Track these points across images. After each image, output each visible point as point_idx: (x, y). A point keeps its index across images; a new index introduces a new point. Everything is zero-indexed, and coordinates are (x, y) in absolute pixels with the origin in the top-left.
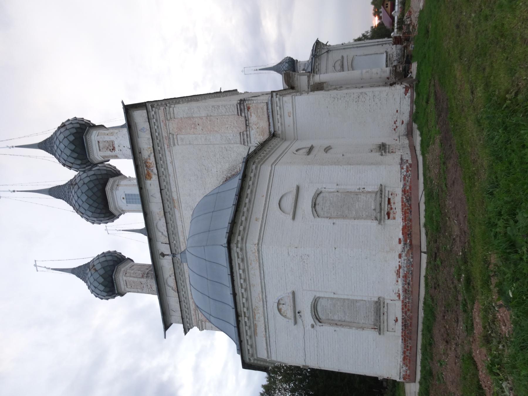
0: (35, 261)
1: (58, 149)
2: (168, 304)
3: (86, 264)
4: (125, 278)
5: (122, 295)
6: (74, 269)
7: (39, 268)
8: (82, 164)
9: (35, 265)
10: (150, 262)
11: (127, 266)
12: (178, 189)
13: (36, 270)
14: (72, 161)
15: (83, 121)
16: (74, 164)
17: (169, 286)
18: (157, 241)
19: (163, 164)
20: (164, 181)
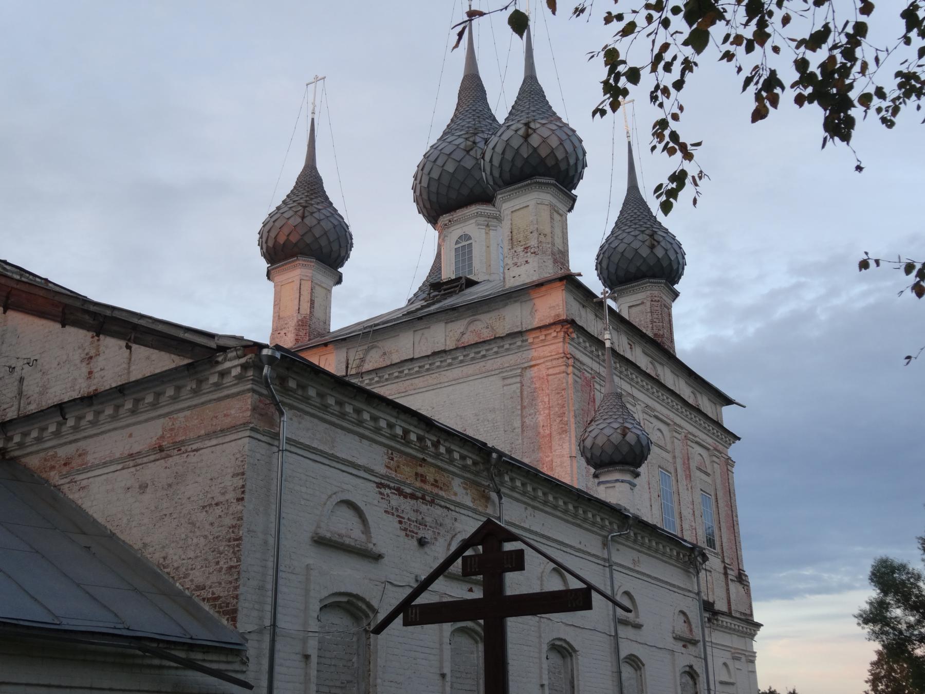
0: (324, 78)
1: (447, 144)
2: (398, 335)
3: (544, 97)
4: (532, 204)
5: (269, 276)
6: (315, 168)
7: (312, 87)
8: (429, 193)
9: (317, 79)
10: (336, 325)
11: (562, 207)
12: (424, 390)
13: (308, 82)
14: (497, 149)
15: (583, 168)
16: (492, 151)
17: (367, 351)
18: (415, 331)
19: (480, 355)
20: (453, 359)
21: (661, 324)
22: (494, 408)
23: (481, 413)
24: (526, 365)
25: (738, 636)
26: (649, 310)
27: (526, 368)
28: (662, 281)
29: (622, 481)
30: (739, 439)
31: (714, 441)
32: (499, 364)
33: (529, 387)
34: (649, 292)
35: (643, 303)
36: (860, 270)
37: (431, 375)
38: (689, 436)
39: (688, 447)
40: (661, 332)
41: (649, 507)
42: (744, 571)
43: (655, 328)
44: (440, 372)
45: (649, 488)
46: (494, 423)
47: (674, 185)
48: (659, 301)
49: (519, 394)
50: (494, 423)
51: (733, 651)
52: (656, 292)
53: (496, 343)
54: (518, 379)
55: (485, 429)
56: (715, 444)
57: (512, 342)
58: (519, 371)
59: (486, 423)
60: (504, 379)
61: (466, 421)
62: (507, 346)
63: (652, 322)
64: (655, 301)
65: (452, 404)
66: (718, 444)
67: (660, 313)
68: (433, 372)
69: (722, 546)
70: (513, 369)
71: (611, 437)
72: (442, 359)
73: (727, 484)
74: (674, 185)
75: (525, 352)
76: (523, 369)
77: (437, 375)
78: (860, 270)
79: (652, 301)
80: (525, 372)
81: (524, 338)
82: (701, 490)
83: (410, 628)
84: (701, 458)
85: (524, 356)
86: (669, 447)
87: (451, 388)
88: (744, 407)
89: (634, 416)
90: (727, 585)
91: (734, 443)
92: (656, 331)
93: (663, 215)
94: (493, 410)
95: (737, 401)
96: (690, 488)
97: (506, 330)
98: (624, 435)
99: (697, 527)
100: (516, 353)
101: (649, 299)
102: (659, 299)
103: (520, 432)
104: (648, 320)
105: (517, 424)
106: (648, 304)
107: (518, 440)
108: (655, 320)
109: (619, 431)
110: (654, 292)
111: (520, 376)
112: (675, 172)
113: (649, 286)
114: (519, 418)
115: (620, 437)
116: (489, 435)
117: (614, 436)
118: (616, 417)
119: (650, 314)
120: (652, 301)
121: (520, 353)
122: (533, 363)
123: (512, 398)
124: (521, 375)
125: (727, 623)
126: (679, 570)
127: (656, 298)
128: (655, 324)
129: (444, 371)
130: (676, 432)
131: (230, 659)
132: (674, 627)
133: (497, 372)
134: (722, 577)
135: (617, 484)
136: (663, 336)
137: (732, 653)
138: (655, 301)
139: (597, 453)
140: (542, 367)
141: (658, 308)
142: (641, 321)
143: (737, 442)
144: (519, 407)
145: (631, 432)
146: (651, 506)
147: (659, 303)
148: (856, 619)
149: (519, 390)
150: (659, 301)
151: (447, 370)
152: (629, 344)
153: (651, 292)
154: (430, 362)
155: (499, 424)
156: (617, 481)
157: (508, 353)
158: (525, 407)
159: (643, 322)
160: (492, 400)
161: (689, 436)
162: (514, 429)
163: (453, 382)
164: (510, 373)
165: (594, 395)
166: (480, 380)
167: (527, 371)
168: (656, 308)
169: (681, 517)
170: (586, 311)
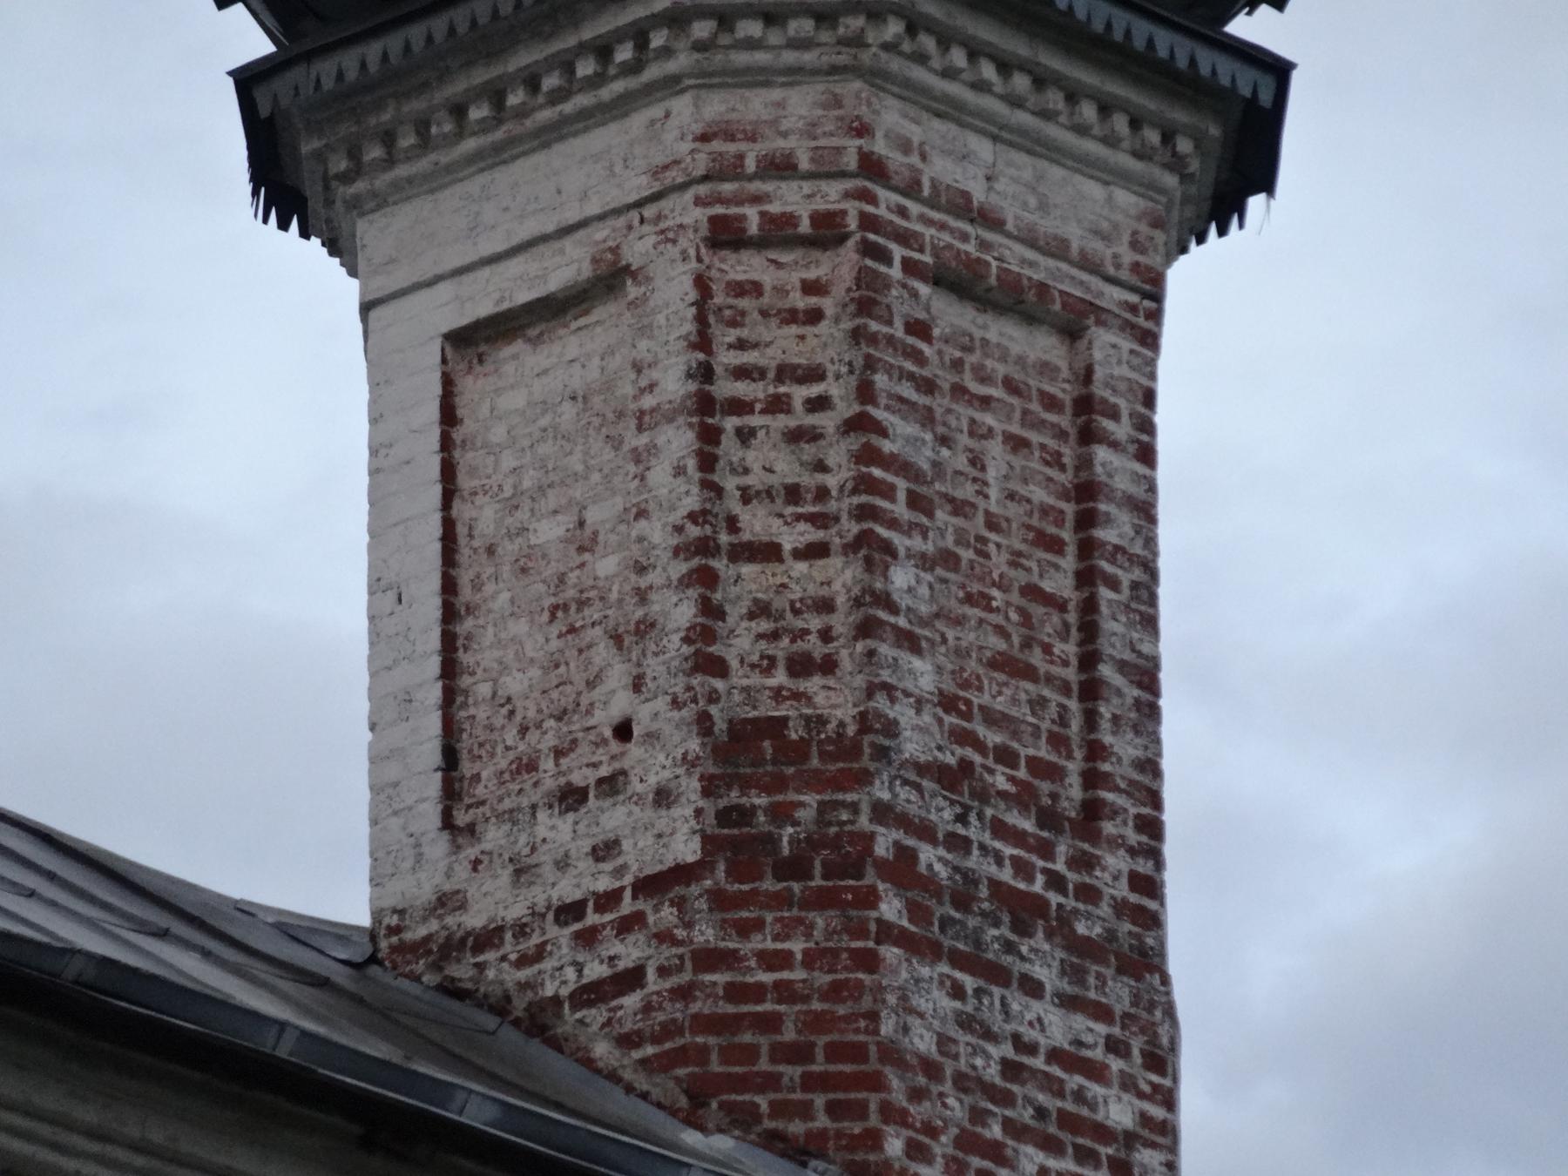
26: (673, 384)
36: (230, 73)
47: (918, 1125)
48: (828, 230)
52: (801, 103)
64: (779, 232)
67: (845, 408)
74: (918, 1125)
78: (230, 73)
83: (229, 86)
89: (474, 920)
101: (687, 212)
102: (832, 194)
104: (657, 532)
108: (757, 523)
110: (755, 104)
112: (1249, 13)
119: (678, 441)
128: (751, 579)
138: (779, 232)
147: (840, 266)
148: (505, 1024)
150: (828, 230)
153: (716, 106)
159: (606, 565)
168: (783, 344)
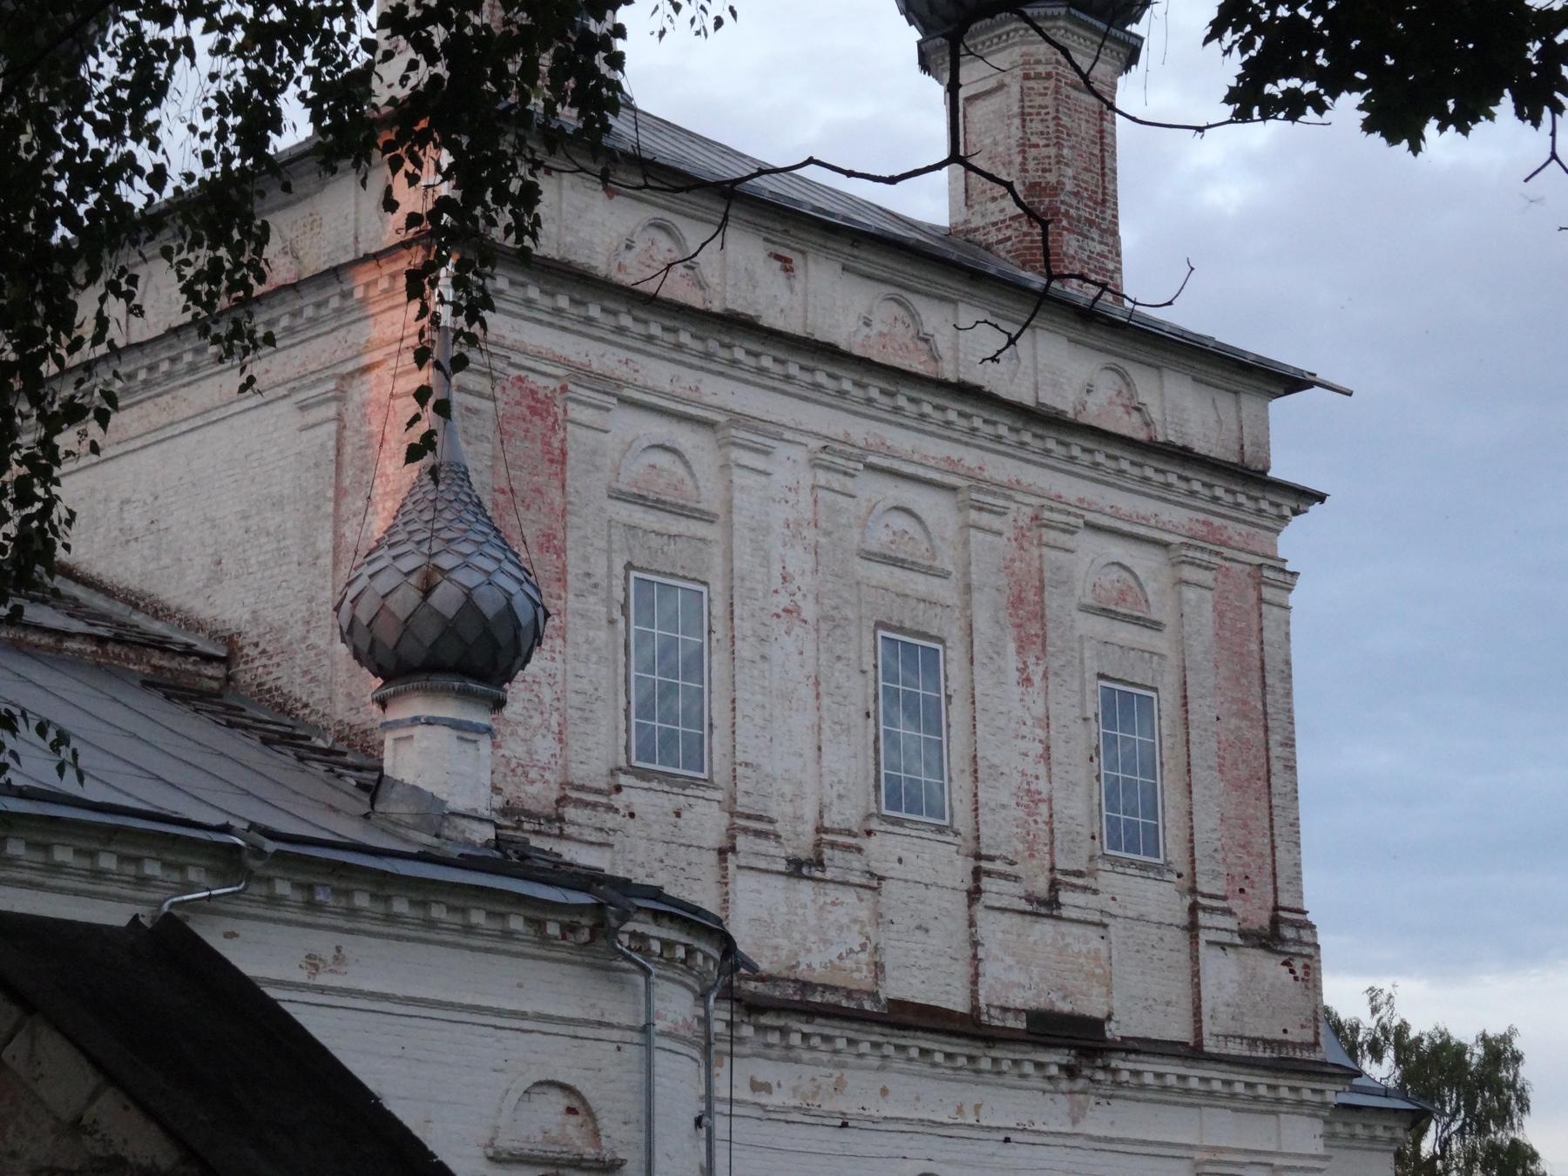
21: (1052, 151)
22: (282, 496)
23: (254, 511)
24: (350, 366)
25: (1236, 1110)
26: (1016, 109)
27: (351, 375)
28: (1056, 11)
29: (430, 722)
30: (1321, 498)
31: (1202, 516)
32: (297, 363)
33: (357, 431)
34: (1017, 50)
35: (1001, 87)
37: (158, 400)
38: (1047, 514)
39: (1045, 550)
40: (1052, 178)
41: (810, 753)
42: (1305, 913)
43: (1031, 165)
44: (173, 389)
45: (818, 696)
46: (279, 541)
48: (1049, 76)
49: (332, 454)
50: (279, 541)
51: (1198, 1156)
53: (283, 302)
54: (331, 410)
55: (261, 558)
56: (1205, 523)
57: (320, 298)
58: (331, 385)
59: (263, 540)
60: (303, 407)
61: (224, 533)
62: (309, 312)
63: (1025, 146)
64: (1038, 76)
65: (194, 485)
66: (1217, 521)
67: (1053, 114)
68: (159, 390)
69: (1191, 841)
70: (319, 380)
71: (390, 598)
72: (173, 353)
73: (1254, 647)
75: (353, 327)
76: (343, 377)
77: (167, 398)
79: (1027, 77)
80: (350, 386)
81: (346, 287)
82: (1101, 676)
84: (1125, 575)
85: (350, 339)
86: (945, 561)
87: (194, 437)
88: (1350, 394)
90: (1195, 959)
91: (1296, 512)
92: (1033, 176)
93: (201, 29)
94: (278, 504)
95: (1321, 376)
96: (1037, 679)
97: (323, 259)
98: (427, 590)
99: (1057, 795)
100: (333, 330)
101: (1019, 72)
102: (1049, 68)
103: (330, 567)
105: (325, 542)
106: (1015, 89)
107: (323, 588)
108: (1034, 139)
109: (414, 580)
110: (1032, 49)
111: (335, 399)
113: (1016, 30)
114: (329, 524)
115: (414, 597)
116: (268, 573)
117: (398, 595)
118: (463, 526)
119: (1017, 122)
120: (1027, 77)
121: (342, 333)
122: (365, 360)
123: (317, 465)
124: (340, 397)
125: (1159, 1076)
126: (567, 968)
127: (1041, 69)
128: (1033, 152)
129: (184, 386)
130: (980, 509)
131: (906, 1033)
132: (496, 1129)
133: (281, 391)
134: (1179, 939)
135: (418, 731)
136: (1056, 189)
137: (1197, 1164)
138: (1038, 76)
139: (388, 635)
140: (383, 373)
141: (1049, 100)
142: (995, 143)
143: (1316, 508)
144: (330, 493)
145: (450, 580)
146: (819, 749)
147: (1051, 83)
149: (332, 443)
151: (189, 384)
152: (778, 257)
153: (1024, 49)
154: (147, 362)
155: (288, 542)
156: (415, 721)
157: (317, 332)
158: (346, 492)
159: (1001, 149)
160: (277, 472)
161: (1047, 514)
162: (317, 558)
163: (199, 421)
164: (313, 392)
165: (563, 440)
166: (253, 414)
167: (356, 382)
168: (1039, 101)
169: (976, 771)
170: (560, 187)
